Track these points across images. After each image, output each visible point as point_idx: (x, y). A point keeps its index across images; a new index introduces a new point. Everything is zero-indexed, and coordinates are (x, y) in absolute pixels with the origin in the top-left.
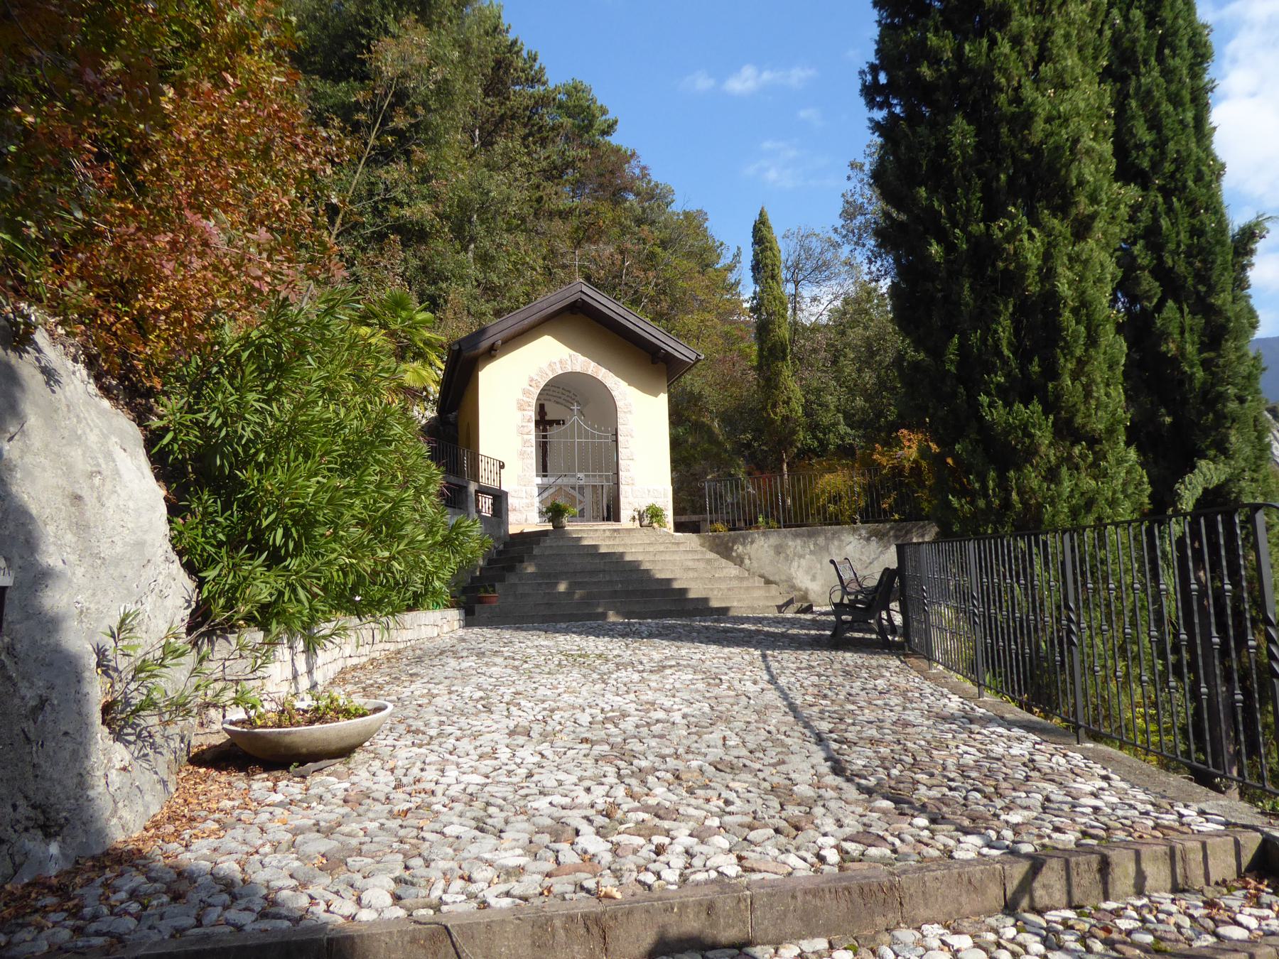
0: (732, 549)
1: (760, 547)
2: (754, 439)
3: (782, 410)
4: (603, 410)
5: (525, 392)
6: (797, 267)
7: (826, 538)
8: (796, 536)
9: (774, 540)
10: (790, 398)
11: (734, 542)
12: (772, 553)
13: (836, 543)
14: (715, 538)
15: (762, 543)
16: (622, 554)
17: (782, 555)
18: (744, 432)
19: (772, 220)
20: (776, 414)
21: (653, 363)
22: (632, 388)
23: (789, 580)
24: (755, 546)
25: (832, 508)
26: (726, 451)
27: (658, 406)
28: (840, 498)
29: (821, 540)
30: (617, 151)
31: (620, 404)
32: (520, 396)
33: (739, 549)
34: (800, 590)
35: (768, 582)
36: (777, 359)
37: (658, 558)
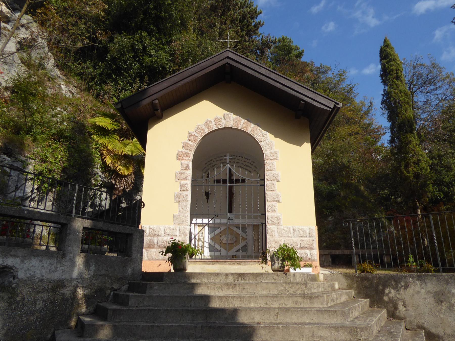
2: (391, 194)
3: (413, 169)
4: (254, 160)
5: (185, 145)
6: (411, 83)
10: (419, 160)
11: (385, 285)
12: (431, 300)
16: (235, 312)
17: (445, 306)
18: (383, 189)
20: (408, 172)
22: (278, 140)
24: (410, 291)
26: (370, 202)
30: (305, 63)
31: (266, 153)
32: (181, 149)
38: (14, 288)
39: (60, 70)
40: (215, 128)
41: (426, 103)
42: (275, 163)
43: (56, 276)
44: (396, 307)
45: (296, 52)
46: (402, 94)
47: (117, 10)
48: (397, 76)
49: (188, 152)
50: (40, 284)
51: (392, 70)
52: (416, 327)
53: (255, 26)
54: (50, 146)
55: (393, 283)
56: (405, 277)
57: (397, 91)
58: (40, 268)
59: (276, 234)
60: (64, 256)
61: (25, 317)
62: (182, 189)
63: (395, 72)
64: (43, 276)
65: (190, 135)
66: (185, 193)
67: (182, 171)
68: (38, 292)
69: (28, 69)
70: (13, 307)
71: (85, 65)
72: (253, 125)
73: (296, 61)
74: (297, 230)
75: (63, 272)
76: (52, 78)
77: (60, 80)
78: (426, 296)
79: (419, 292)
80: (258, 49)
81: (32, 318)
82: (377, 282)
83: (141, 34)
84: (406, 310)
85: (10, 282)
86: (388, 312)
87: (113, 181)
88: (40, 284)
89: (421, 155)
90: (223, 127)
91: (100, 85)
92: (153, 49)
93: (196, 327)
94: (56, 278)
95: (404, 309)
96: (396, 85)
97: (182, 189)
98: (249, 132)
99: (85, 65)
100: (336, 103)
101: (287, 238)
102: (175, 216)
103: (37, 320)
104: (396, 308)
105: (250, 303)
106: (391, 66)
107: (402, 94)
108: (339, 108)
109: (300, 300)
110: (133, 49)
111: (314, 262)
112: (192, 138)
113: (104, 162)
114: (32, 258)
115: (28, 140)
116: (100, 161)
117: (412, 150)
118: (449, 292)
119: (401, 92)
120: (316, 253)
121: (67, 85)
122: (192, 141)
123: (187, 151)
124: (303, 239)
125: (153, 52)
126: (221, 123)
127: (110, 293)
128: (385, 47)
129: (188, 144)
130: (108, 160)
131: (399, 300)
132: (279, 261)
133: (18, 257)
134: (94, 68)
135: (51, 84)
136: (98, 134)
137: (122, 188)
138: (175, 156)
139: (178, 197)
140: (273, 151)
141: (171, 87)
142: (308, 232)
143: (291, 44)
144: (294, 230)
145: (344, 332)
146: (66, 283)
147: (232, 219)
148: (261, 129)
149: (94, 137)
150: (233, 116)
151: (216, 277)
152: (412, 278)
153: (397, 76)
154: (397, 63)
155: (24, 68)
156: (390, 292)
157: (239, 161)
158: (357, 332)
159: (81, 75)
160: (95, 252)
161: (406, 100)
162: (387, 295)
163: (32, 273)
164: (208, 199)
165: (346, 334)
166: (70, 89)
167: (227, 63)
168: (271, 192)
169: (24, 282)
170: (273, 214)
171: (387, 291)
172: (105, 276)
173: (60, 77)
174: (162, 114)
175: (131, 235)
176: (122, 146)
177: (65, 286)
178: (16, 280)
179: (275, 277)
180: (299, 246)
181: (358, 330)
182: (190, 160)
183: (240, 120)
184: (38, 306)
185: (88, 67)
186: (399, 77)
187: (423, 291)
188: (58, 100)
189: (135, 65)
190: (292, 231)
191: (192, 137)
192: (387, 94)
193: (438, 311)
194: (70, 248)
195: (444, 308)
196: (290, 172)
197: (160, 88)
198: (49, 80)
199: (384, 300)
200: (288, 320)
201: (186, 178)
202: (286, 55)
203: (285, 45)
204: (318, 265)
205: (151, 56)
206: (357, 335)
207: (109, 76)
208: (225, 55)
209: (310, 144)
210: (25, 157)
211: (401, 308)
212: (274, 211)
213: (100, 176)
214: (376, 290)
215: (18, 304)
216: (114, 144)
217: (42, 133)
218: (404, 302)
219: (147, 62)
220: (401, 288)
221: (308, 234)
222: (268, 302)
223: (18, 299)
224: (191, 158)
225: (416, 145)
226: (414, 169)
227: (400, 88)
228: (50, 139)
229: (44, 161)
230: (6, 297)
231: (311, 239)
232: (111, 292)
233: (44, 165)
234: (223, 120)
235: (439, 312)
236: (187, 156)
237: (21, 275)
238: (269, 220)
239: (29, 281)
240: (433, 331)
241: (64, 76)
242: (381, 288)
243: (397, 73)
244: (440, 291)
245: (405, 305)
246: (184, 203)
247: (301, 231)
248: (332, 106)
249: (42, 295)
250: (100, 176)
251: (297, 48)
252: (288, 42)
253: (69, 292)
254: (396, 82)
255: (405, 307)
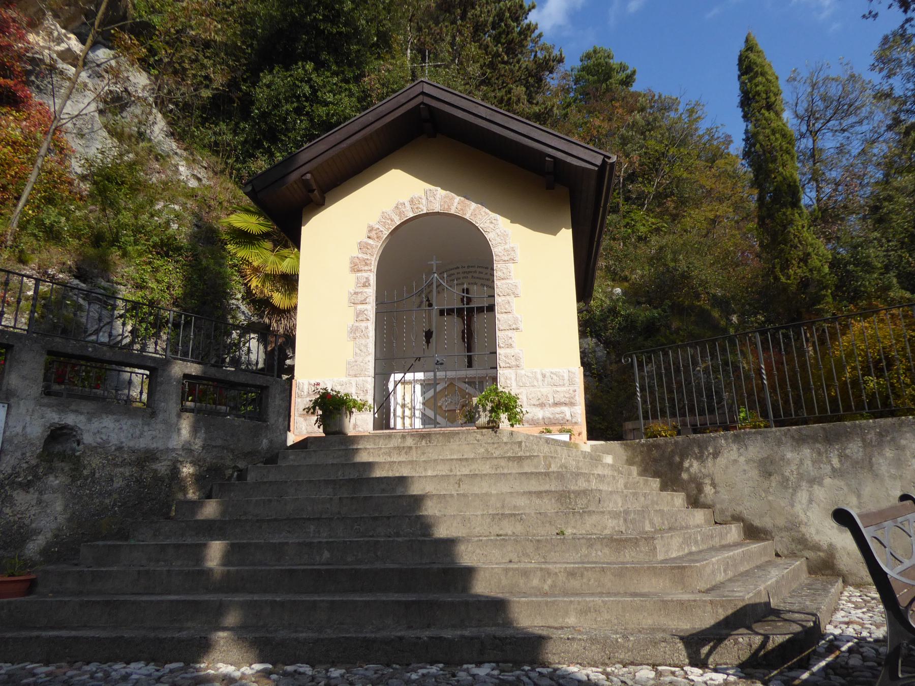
0: (680, 467)
1: (732, 465)
4: (473, 265)
5: (362, 247)
7: (866, 444)
8: (800, 441)
9: (756, 449)
11: (683, 456)
12: (754, 473)
13: (889, 453)
14: (650, 447)
15: (734, 455)
17: (775, 480)
19: (761, 43)
20: (788, 278)
21: (550, 187)
22: (518, 227)
23: (793, 526)
24: (721, 461)
25: (872, 383)
27: (561, 245)
28: (890, 363)
29: (855, 448)
32: (356, 253)
33: (693, 466)
34: (816, 548)
35: (753, 533)
36: (784, 205)
37: (465, 488)
38: (79, 457)
39: (177, 141)
40: (411, 215)
41: (841, 150)
42: (511, 266)
43: (143, 443)
44: (700, 489)
45: (622, 76)
46: (778, 136)
47: (263, 29)
48: (768, 103)
49: (368, 257)
50: (117, 453)
51: (758, 93)
52: (730, 519)
53: (520, 33)
54: (150, 263)
55: (697, 451)
56: (715, 438)
57: (767, 131)
58: (116, 430)
59: (514, 384)
60: (153, 414)
61: (97, 498)
62: (360, 318)
63: (764, 96)
64: (122, 443)
65: (371, 229)
66: (363, 324)
67: (359, 290)
68: (116, 465)
69: (120, 141)
70: (79, 482)
71: (217, 129)
72: (473, 205)
73: (620, 90)
74: (548, 375)
75: (153, 438)
76: (161, 156)
77: (177, 158)
78: (746, 468)
79: (735, 461)
80: (530, 75)
81: (107, 501)
82: (672, 451)
83: (304, 67)
84: (715, 493)
85: (74, 450)
86: (688, 497)
87: (267, 321)
88: (117, 453)
89: (812, 245)
90: (425, 212)
91: (244, 162)
92: (329, 92)
93: (331, 499)
94: (142, 446)
95: (713, 491)
96: (766, 119)
97: (360, 318)
98: (467, 217)
99: (217, 129)
100: (605, 156)
101: (532, 389)
102: (349, 363)
103: (115, 504)
104: (700, 490)
105: (425, 470)
106: (756, 86)
107: (778, 136)
108: (612, 164)
109: (503, 463)
110: (293, 96)
111: (576, 427)
112: (373, 234)
113: (249, 291)
114: (104, 416)
115: (115, 254)
116: (242, 288)
117: (795, 236)
118: (783, 458)
119: (774, 132)
120: (579, 412)
121: (189, 167)
122: (373, 239)
123: (365, 257)
124: (558, 389)
125: (330, 97)
126: (421, 206)
127: (232, 475)
128: (747, 50)
129: (367, 244)
130: (254, 283)
131: (705, 476)
132: (487, 413)
133: (81, 413)
134: (235, 133)
135: (161, 165)
136: (237, 243)
137: (281, 331)
138: (347, 265)
139: (354, 332)
140: (507, 247)
141: (331, 151)
142: (566, 377)
143: (611, 61)
144: (544, 376)
145: (550, 500)
146: (158, 455)
147: (442, 364)
148: (487, 211)
149: (230, 247)
150: (440, 192)
151: (387, 441)
152: (725, 440)
153: (768, 103)
154: (767, 80)
155: (111, 142)
156: (691, 466)
157: (481, 276)
158: (570, 498)
159: (214, 148)
160: (211, 413)
161: (785, 145)
162: (688, 470)
163: (104, 438)
164: (428, 342)
165: (553, 501)
166: (195, 172)
167: (422, 103)
168: (505, 316)
169: (94, 449)
170: (508, 351)
171: (686, 464)
172: (223, 448)
173: (176, 153)
174: (324, 199)
175: (267, 388)
176: (277, 260)
177: (157, 459)
178: (81, 446)
179: (479, 437)
180: (551, 401)
181: (572, 496)
182: (370, 270)
183: (453, 199)
184: (116, 485)
185: (224, 132)
186: (771, 105)
187: (742, 459)
188: (171, 189)
189: (301, 121)
190: (540, 377)
191: (374, 232)
192: (750, 139)
193: (764, 491)
194: (163, 404)
195: (773, 484)
196: (536, 280)
197: (314, 154)
198: (157, 160)
199: (682, 479)
200: (476, 490)
201: (365, 300)
202: (600, 82)
203: (599, 64)
204: (582, 427)
205: (326, 104)
206: (570, 503)
207: (258, 145)
208: (418, 89)
209: (571, 230)
210: (108, 281)
211: (708, 490)
212: (510, 346)
213: (244, 312)
214: (671, 464)
215: (86, 480)
216: (262, 257)
217: (136, 242)
218: (712, 479)
219: (319, 116)
220: (707, 457)
221: (566, 382)
222: (453, 467)
223: (85, 472)
224: (374, 267)
225: (803, 227)
226: (799, 271)
227: (772, 125)
228: (151, 252)
229: (140, 287)
230: (67, 469)
231: (572, 388)
232: (233, 472)
233: (140, 293)
234: (424, 201)
235: (766, 491)
236: (366, 264)
237: (88, 439)
238: (501, 362)
239: (99, 448)
240: (757, 523)
241: (185, 150)
242: (677, 459)
243: (768, 98)
244: (767, 458)
245: (714, 485)
246: (363, 342)
247: (554, 377)
248: (599, 162)
249: (121, 470)
250: (243, 313)
251: (623, 68)
252: (605, 58)
253: (164, 469)
254: (767, 114)
255: (714, 488)
